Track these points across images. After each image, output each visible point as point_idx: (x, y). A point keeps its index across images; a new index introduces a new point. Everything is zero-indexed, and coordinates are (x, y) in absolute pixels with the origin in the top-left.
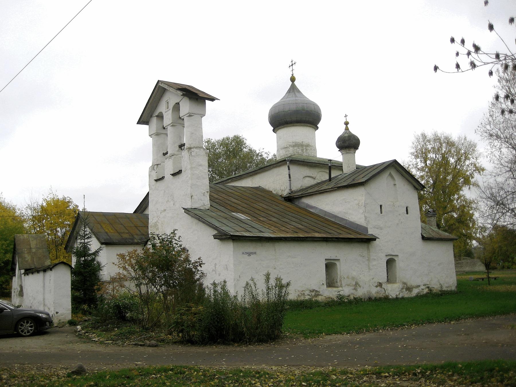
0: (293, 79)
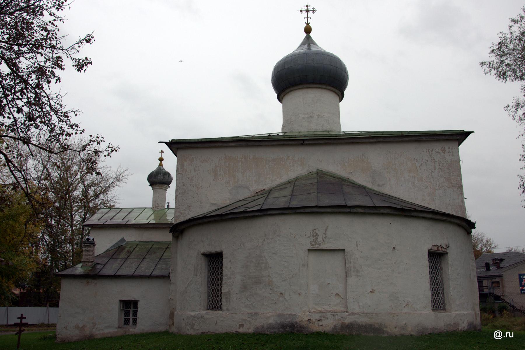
0: (308, 30)
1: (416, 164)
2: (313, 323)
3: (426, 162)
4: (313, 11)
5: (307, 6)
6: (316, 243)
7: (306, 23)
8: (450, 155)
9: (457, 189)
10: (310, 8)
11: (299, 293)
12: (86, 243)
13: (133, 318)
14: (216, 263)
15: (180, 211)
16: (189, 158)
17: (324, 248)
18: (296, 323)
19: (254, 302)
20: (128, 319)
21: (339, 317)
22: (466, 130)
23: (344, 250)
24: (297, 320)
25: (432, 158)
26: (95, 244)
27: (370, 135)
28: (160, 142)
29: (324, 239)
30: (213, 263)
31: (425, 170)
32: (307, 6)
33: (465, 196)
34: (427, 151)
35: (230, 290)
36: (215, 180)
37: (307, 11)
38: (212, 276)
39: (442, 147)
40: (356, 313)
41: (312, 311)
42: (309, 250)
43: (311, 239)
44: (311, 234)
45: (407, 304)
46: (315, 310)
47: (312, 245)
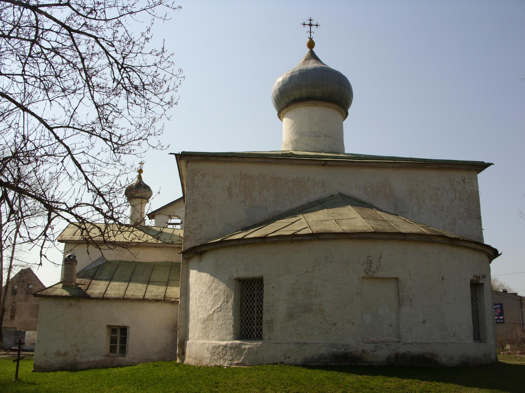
0: (311, 44)
1: (437, 192)
2: (367, 354)
3: (447, 192)
4: (317, 25)
5: (310, 20)
6: (370, 271)
7: (309, 38)
8: (469, 186)
9: (476, 220)
10: (313, 23)
11: (352, 323)
12: (68, 261)
13: (121, 346)
14: (251, 289)
15: (190, 230)
16: (201, 173)
17: (378, 276)
18: (350, 353)
19: (302, 332)
20: (114, 346)
21: (393, 348)
22: (486, 162)
23: (397, 279)
24: (351, 350)
25: (453, 188)
26: (76, 262)
27: (426, 162)
28: (171, 154)
29: (378, 266)
30: (247, 289)
31: (446, 199)
32: (310, 20)
33: (483, 227)
34: (449, 180)
35: (273, 318)
36: (229, 198)
37: (310, 25)
38: (246, 303)
39: (463, 178)
40: (409, 343)
41: (365, 341)
42: (363, 278)
43: (365, 266)
44: (365, 261)
45: (454, 334)
46: (368, 340)
47: (366, 273)
